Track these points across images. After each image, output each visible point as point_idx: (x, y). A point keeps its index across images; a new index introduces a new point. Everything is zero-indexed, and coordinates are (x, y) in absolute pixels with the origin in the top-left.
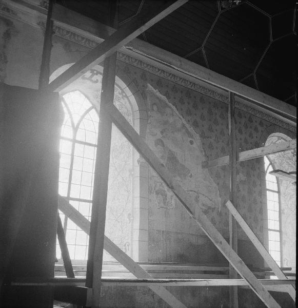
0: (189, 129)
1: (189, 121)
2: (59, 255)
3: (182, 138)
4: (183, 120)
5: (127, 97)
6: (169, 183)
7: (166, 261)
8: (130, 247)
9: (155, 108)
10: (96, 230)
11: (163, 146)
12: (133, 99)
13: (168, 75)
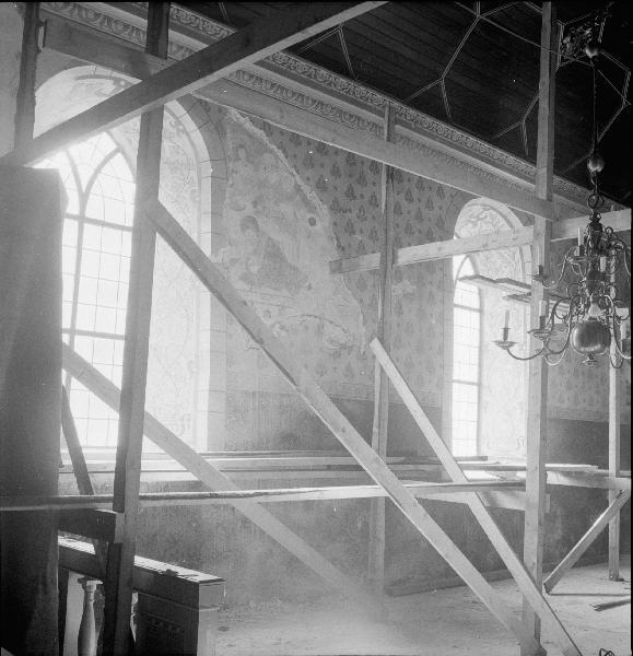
0: (309, 195)
1: (308, 179)
2: (64, 451)
3: (295, 214)
4: (298, 178)
5: (187, 134)
6: (255, 334)
7: (257, 448)
8: (192, 422)
9: (242, 153)
10: (130, 401)
11: (257, 229)
12: (198, 137)
13: (269, 86)
